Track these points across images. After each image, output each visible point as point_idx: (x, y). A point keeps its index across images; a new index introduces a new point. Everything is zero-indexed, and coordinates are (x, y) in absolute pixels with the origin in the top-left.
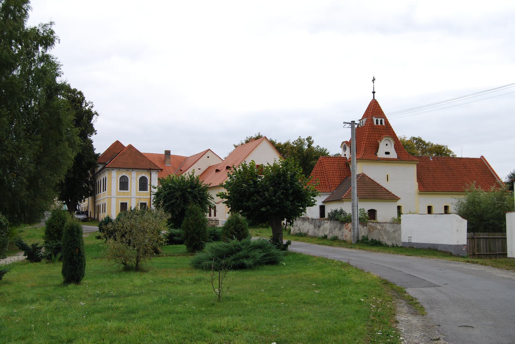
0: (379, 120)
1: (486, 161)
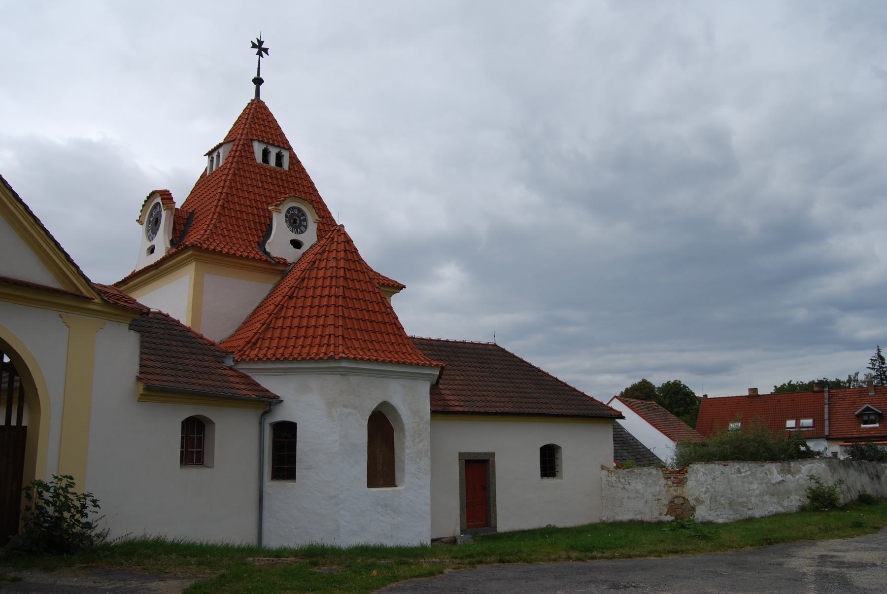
0: (273, 152)
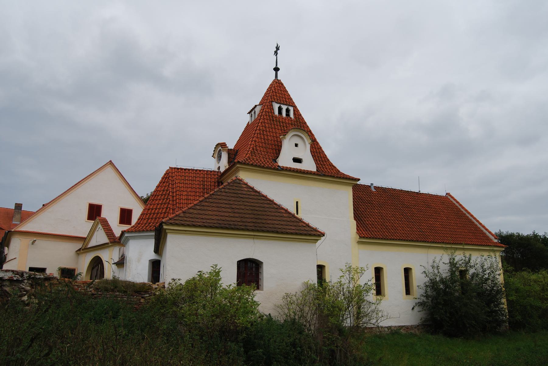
0: (284, 108)
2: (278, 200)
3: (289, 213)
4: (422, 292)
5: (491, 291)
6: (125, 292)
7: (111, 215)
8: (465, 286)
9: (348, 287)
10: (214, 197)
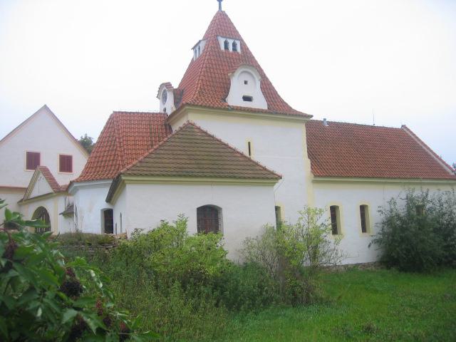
0: (231, 42)
1: (411, 132)
2: (233, 144)
3: (245, 157)
4: (379, 230)
5: (448, 225)
6: (90, 244)
7: (50, 162)
8: (422, 224)
9: (307, 229)
10: (168, 144)
